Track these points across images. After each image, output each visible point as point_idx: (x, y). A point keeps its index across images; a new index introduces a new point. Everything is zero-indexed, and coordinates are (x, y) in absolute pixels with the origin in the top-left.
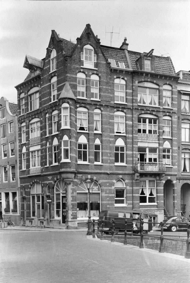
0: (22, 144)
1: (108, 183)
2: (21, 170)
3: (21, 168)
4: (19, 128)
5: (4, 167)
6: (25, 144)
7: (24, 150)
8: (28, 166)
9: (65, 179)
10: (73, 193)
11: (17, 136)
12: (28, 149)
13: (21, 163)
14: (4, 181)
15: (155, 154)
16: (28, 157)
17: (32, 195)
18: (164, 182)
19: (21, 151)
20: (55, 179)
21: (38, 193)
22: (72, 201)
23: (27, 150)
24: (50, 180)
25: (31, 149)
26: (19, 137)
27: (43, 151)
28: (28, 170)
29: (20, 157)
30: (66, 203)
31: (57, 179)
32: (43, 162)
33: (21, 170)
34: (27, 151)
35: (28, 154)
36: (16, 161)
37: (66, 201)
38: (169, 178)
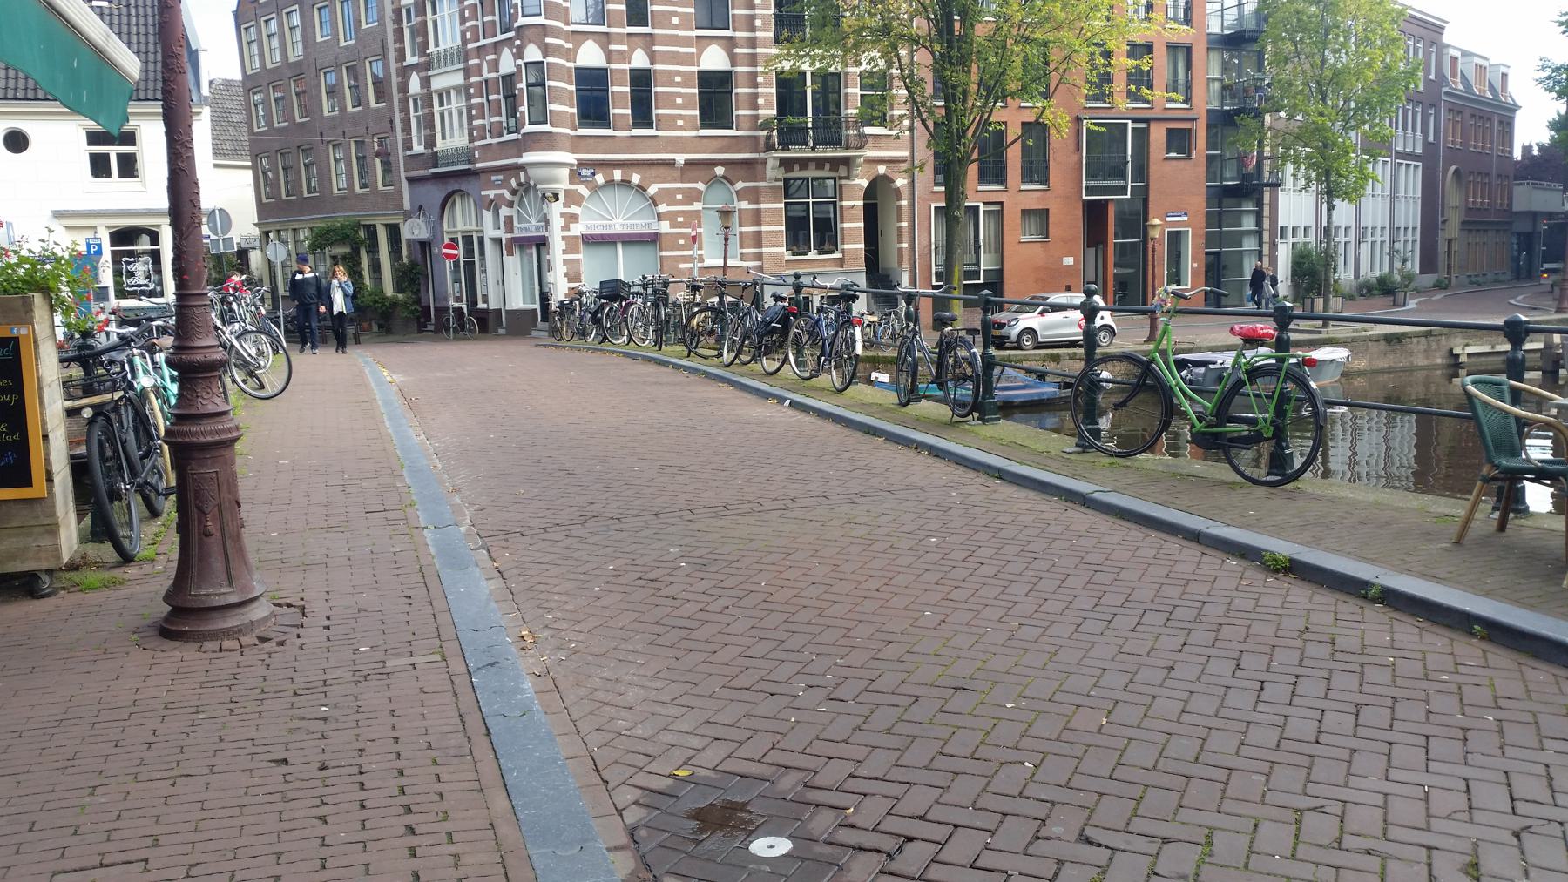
0: (405, 64)
1: (678, 83)
2: (408, 153)
3: (408, 146)
4: (393, 11)
5: (347, 68)
6: (414, 67)
7: (415, 85)
8: (430, 142)
9: (542, 183)
10: (566, 228)
11: (390, 37)
12: (426, 82)
13: (407, 129)
14: (350, 109)
15: (846, 82)
16: (426, 111)
17: (448, 233)
18: (865, 183)
19: (404, 88)
20: (513, 183)
21: (468, 228)
22: (564, 252)
23: (422, 87)
24: (499, 187)
25: (437, 84)
26: (395, 42)
27: (472, 91)
28: (430, 151)
29: (405, 109)
30: (547, 234)
31: (520, 184)
32: (469, 29)
33: (408, 153)
34: (425, 91)
35: (427, 100)
36: (392, 122)
37: (547, 230)
38: (882, 169)
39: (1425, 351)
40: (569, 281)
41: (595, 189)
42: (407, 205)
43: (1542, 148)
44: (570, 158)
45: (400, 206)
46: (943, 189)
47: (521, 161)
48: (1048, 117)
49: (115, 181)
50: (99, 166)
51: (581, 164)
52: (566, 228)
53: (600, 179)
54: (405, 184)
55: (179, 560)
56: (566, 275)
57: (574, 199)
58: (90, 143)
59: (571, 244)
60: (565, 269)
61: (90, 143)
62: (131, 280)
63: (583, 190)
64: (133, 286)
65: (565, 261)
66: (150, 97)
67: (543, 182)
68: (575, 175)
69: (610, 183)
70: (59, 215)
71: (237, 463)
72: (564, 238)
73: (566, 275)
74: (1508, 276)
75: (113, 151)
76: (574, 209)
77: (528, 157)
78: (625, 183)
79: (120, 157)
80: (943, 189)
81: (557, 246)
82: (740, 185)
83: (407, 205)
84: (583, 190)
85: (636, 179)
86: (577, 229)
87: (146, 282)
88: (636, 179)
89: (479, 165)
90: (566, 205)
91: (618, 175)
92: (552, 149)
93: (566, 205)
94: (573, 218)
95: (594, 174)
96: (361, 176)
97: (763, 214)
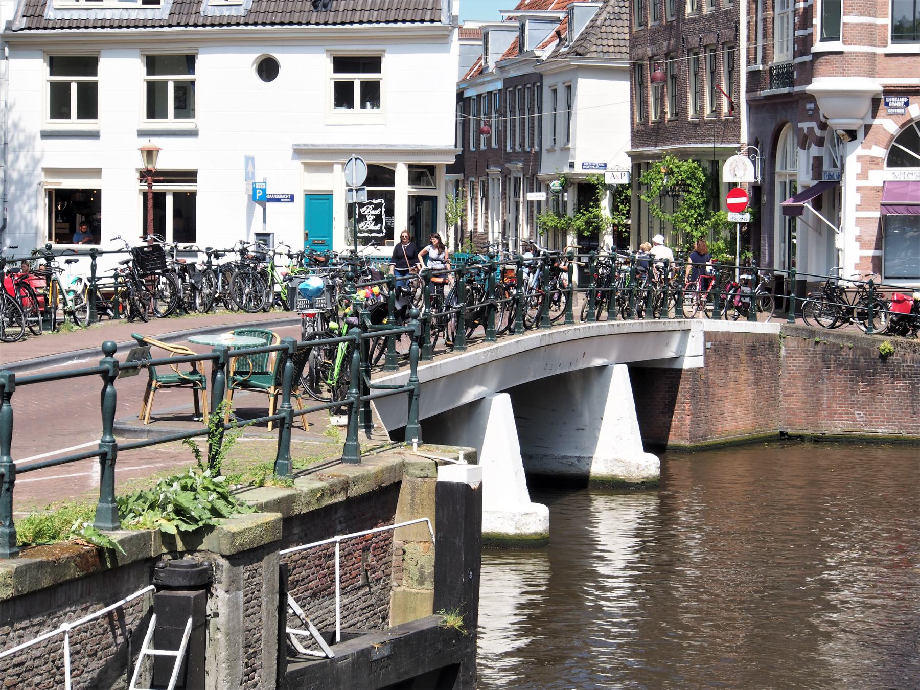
10: (863, 175)
22: (859, 208)
40: (862, 248)
46: (478, 661)
48: (860, 310)
49: (357, 114)
50: (343, 95)
55: (479, 575)
56: (858, 239)
58: (337, 70)
60: (857, 231)
61: (337, 70)
62: (363, 224)
64: (365, 232)
66: (427, 18)
71: (464, 480)
72: (859, 189)
73: (858, 239)
75: (357, 78)
80: (478, 661)
87: (377, 228)
95: (907, 104)
97: (873, 246)
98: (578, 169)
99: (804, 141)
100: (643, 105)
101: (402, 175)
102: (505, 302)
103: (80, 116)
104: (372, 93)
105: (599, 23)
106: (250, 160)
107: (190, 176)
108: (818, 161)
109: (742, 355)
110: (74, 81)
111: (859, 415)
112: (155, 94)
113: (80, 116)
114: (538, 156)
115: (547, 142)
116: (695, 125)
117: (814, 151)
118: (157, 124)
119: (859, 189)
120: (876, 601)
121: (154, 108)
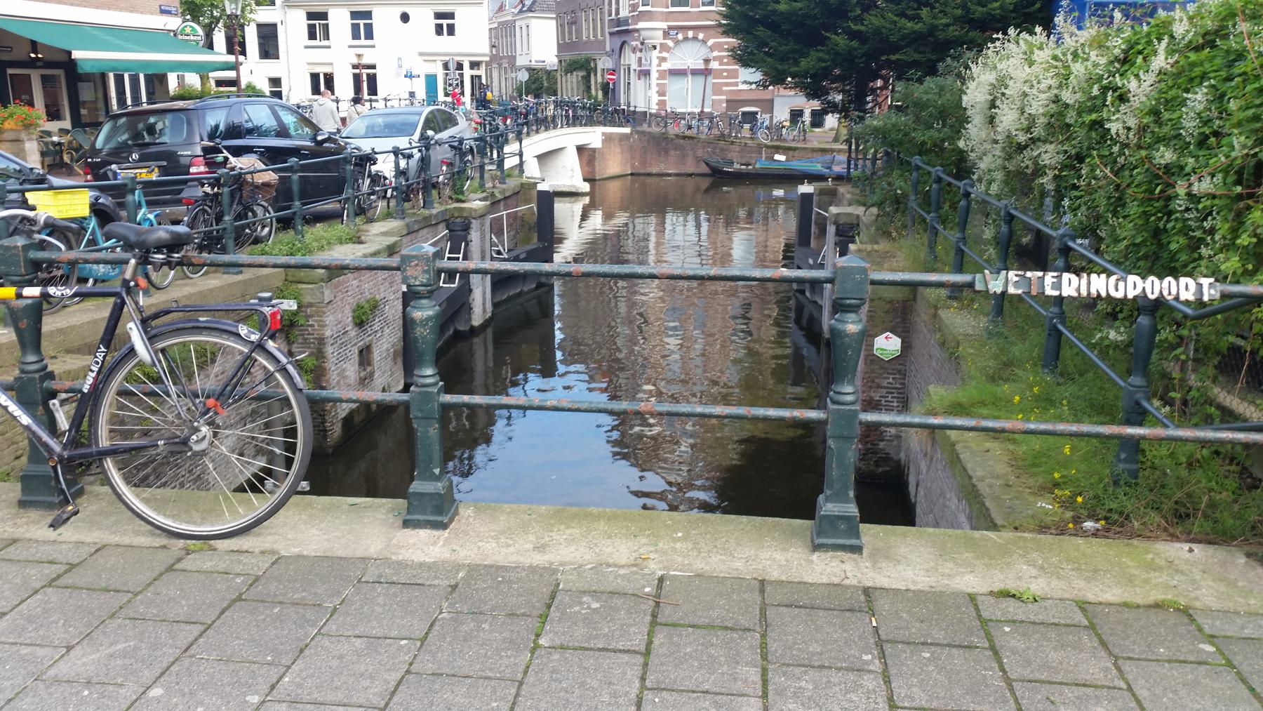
10: (659, 65)
39: (541, 616)
41: (677, 42)
42: (608, 48)
43: (803, 183)
44: (664, 25)
45: (604, 49)
47: (637, 27)
51: (670, 28)
52: (659, 65)
53: (680, 37)
54: (607, 36)
57: (664, 48)
58: (308, 19)
59: (662, 74)
60: (657, 89)
61: (308, 19)
63: (670, 43)
65: (658, 85)
67: (649, 39)
68: (666, 34)
69: (686, 39)
70: (421, 54)
74: (979, 598)
75: (445, 22)
76: (665, 54)
77: (641, 25)
78: (695, 38)
79: (448, 25)
81: (654, 75)
82: (710, 43)
83: (608, 48)
84: (670, 43)
85: (701, 36)
86: (665, 66)
88: (701, 36)
89: (631, 27)
90: (660, 52)
91: (690, 34)
92: (651, 20)
93: (660, 52)
94: (663, 59)
96: (576, 34)
98: (533, 63)
99: (634, 50)
100: (563, 33)
101: (466, 66)
102: (498, 136)
103: (366, 38)
104: (451, 29)
105: (1165, 218)
106: (399, 59)
107: (373, 67)
108: (640, 59)
109: (616, 141)
110: (362, 22)
111: (662, 165)
112: (355, 28)
113: (366, 38)
114: (515, 57)
115: (518, 52)
116: (586, 43)
117: (639, 54)
118: (313, 43)
119: (658, 85)
120: (683, 408)
121: (356, 35)
